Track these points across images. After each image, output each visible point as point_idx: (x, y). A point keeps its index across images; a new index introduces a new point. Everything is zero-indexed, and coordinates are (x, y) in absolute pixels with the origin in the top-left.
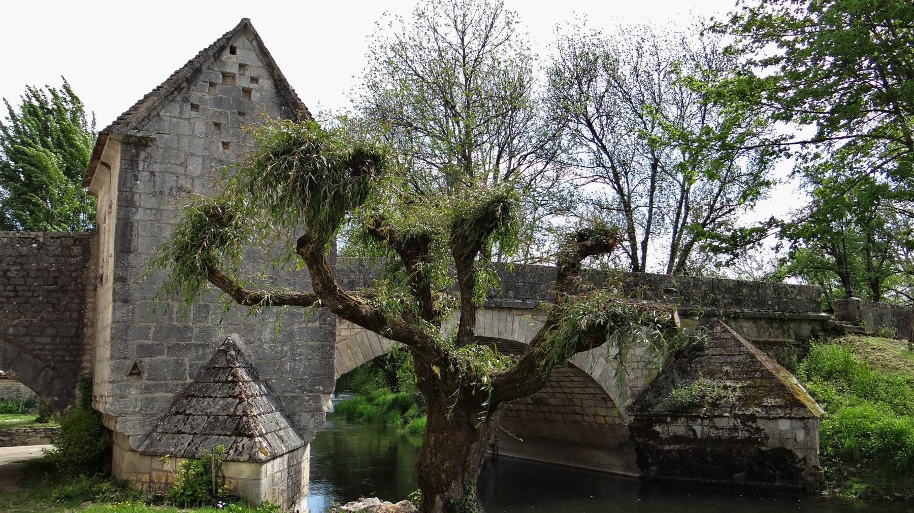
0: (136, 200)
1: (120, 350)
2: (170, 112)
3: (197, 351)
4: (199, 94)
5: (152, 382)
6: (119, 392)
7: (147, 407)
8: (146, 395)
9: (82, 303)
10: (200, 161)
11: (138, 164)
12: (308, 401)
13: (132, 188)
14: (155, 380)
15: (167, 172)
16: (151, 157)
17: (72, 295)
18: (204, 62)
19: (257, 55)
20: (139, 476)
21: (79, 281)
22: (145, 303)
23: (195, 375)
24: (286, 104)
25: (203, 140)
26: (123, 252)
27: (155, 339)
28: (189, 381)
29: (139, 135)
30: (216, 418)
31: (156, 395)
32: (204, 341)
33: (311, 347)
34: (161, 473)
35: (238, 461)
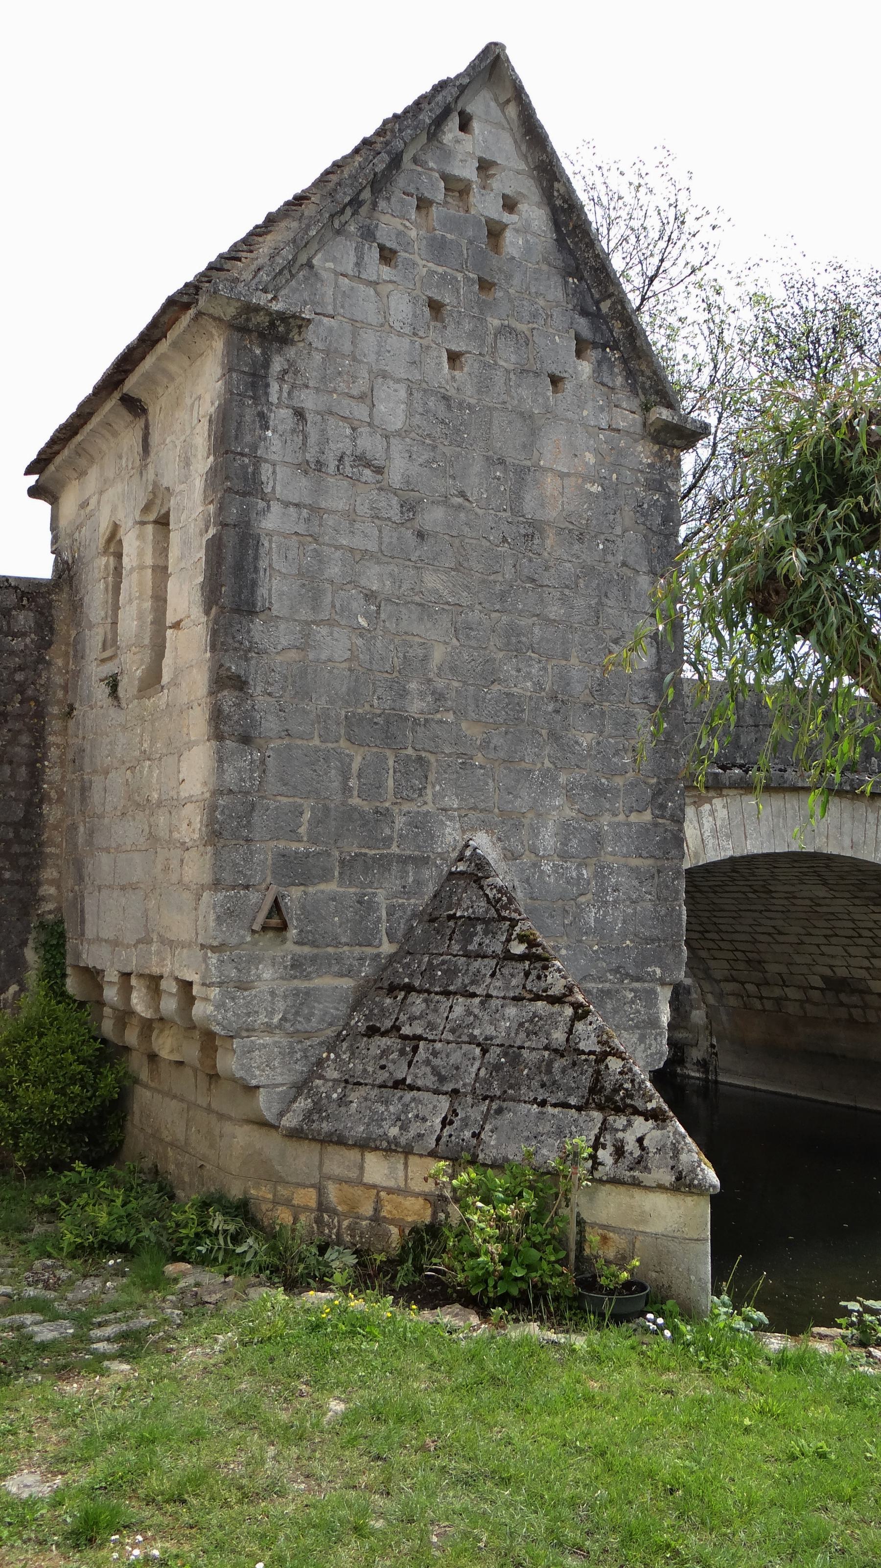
0: (264, 478)
1: (236, 865)
2: (334, 260)
3: (404, 875)
4: (397, 223)
5: (306, 950)
6: (233, 973)
7: (297, 1013)
8: (296, 983)
9: (37, 746)
10: (403, 394)
11: (267, 385)
12: (633, 1002)
13: (255, 447)
14: (313, 944)
15: (331, 413)
16: (297, 372)
17: (18, 726)
18: (413, 139)
19: (515, 142)
20: (283, 1191)
21: (30, 692)
22: (289, 747)
23: (400, 934)
24: (576, 272)
25: (406, 341)
26: (237, 610)
27: (313, 840)
28: (387, 948)
29: (277, 306)
30: (513, 1054)
31: (317, 982)
32: (419, 847)
33: (635, 870)
34: (358, 1191)
35: (636, 1184)
